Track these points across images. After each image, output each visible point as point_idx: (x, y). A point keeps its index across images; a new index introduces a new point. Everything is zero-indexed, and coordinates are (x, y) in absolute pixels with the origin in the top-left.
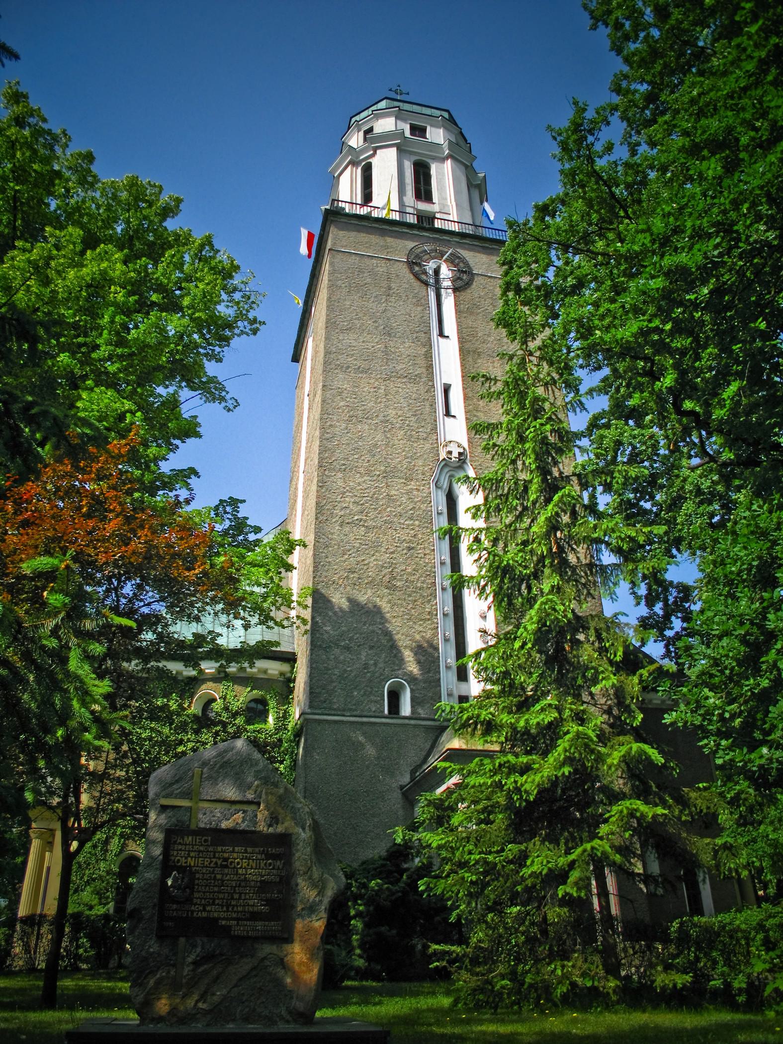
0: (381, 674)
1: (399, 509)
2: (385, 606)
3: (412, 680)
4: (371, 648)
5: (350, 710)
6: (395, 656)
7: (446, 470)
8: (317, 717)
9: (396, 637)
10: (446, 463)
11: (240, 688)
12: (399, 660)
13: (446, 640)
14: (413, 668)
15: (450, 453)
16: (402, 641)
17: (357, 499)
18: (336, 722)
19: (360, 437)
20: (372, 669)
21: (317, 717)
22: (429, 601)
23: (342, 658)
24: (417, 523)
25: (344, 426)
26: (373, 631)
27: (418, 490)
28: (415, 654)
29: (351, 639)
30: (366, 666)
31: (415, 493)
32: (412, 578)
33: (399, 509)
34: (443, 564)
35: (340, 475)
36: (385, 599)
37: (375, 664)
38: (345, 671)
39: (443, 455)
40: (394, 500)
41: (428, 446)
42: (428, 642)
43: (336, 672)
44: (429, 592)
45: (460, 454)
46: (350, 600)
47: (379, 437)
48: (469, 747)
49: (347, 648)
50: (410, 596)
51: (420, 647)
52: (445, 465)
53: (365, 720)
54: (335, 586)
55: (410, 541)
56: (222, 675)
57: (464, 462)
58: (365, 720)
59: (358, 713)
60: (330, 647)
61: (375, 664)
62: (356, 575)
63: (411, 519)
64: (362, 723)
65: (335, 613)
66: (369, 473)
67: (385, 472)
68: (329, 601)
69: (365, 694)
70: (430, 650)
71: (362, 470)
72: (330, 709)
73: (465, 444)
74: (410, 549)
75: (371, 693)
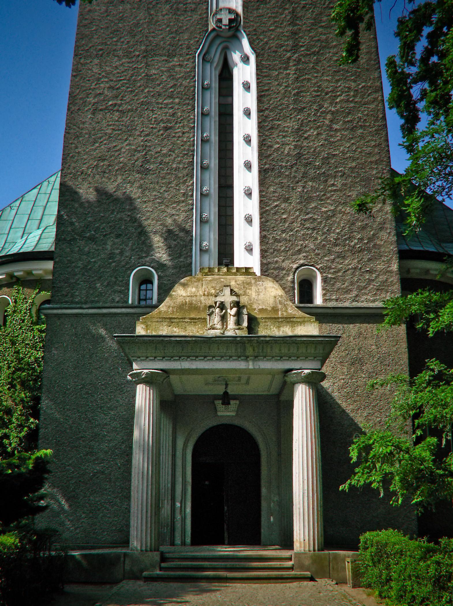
0: (127, 263)
1: (158, 89)
2: (134, 192)
3: (160, 266)
4: (118, 236)
5: (92, 302)
6: (144, 243)
7: (218, 42)
8: (55, 311)
9: (146, 223)
10: (217, 34)
11: (29, 290)
12: (147, 248)
13: (203, 222)
14: (161, 254)
15: (220, 20)
16: (151, 224)
17: (112, 84)
18: (76, 315)
19: (121, 19)
20: (118, 258)
21: (55, 311)
22: (185, 182)
23: (86, 249)
24: (177, 100)
25: (104, 8)
26: (121, 219)
27: (180, 66)
28: (165, 239)
29: (97, 230)
30: (111, 256)
31: (177, 69)
32: (167, 160)
33: (158, 89)
34: (204, 141)
35: (96, 61)
36: (136, 185)
37: (121, 253)
38: (89, 262)
39: (212, 25)
40: (153, 80)
41: (196, 17)
42: (179, 226)
43: (80, 264)
44: (185, 172)
45: (231, 21)
46: (97, 190)
47: (141, 15)
48: (149, 333)
49: (92, 239)
50: (164, 178)
51: (170, 232)
52: (217, 36)
53: (105, 311)
54: (83, 176)
55: (169, 121)
56: (14, 280)
57: (237, 30)
58: (105, 311)
59: (100, 305)
60: (75, 239)
61: (121, 253)
62: (106, 163)
63: (171, 97)
64: (104, 315)
65: (81, 205)
66: (128, 54)
67: (146, 51)
68: (76, 193)
69: (108, 284)
70: (182, 234)
71: (120, 53)
72: (72, 302)
73: (240, 10)
74: (166, 129)
75: (115, 282)
